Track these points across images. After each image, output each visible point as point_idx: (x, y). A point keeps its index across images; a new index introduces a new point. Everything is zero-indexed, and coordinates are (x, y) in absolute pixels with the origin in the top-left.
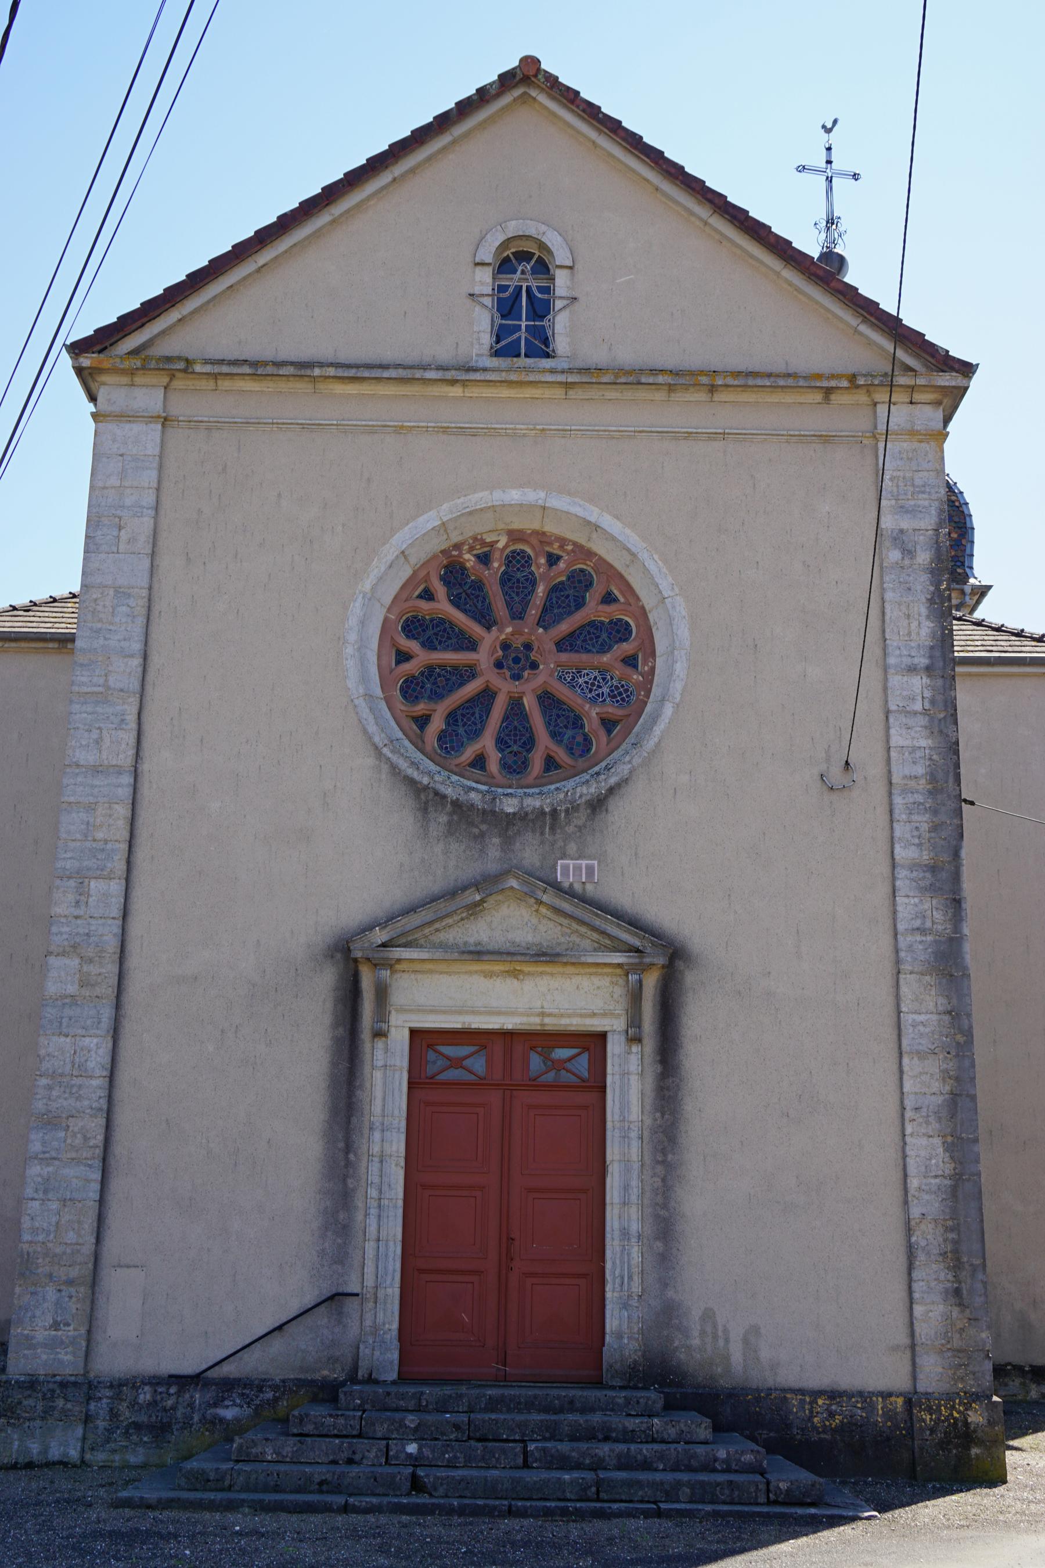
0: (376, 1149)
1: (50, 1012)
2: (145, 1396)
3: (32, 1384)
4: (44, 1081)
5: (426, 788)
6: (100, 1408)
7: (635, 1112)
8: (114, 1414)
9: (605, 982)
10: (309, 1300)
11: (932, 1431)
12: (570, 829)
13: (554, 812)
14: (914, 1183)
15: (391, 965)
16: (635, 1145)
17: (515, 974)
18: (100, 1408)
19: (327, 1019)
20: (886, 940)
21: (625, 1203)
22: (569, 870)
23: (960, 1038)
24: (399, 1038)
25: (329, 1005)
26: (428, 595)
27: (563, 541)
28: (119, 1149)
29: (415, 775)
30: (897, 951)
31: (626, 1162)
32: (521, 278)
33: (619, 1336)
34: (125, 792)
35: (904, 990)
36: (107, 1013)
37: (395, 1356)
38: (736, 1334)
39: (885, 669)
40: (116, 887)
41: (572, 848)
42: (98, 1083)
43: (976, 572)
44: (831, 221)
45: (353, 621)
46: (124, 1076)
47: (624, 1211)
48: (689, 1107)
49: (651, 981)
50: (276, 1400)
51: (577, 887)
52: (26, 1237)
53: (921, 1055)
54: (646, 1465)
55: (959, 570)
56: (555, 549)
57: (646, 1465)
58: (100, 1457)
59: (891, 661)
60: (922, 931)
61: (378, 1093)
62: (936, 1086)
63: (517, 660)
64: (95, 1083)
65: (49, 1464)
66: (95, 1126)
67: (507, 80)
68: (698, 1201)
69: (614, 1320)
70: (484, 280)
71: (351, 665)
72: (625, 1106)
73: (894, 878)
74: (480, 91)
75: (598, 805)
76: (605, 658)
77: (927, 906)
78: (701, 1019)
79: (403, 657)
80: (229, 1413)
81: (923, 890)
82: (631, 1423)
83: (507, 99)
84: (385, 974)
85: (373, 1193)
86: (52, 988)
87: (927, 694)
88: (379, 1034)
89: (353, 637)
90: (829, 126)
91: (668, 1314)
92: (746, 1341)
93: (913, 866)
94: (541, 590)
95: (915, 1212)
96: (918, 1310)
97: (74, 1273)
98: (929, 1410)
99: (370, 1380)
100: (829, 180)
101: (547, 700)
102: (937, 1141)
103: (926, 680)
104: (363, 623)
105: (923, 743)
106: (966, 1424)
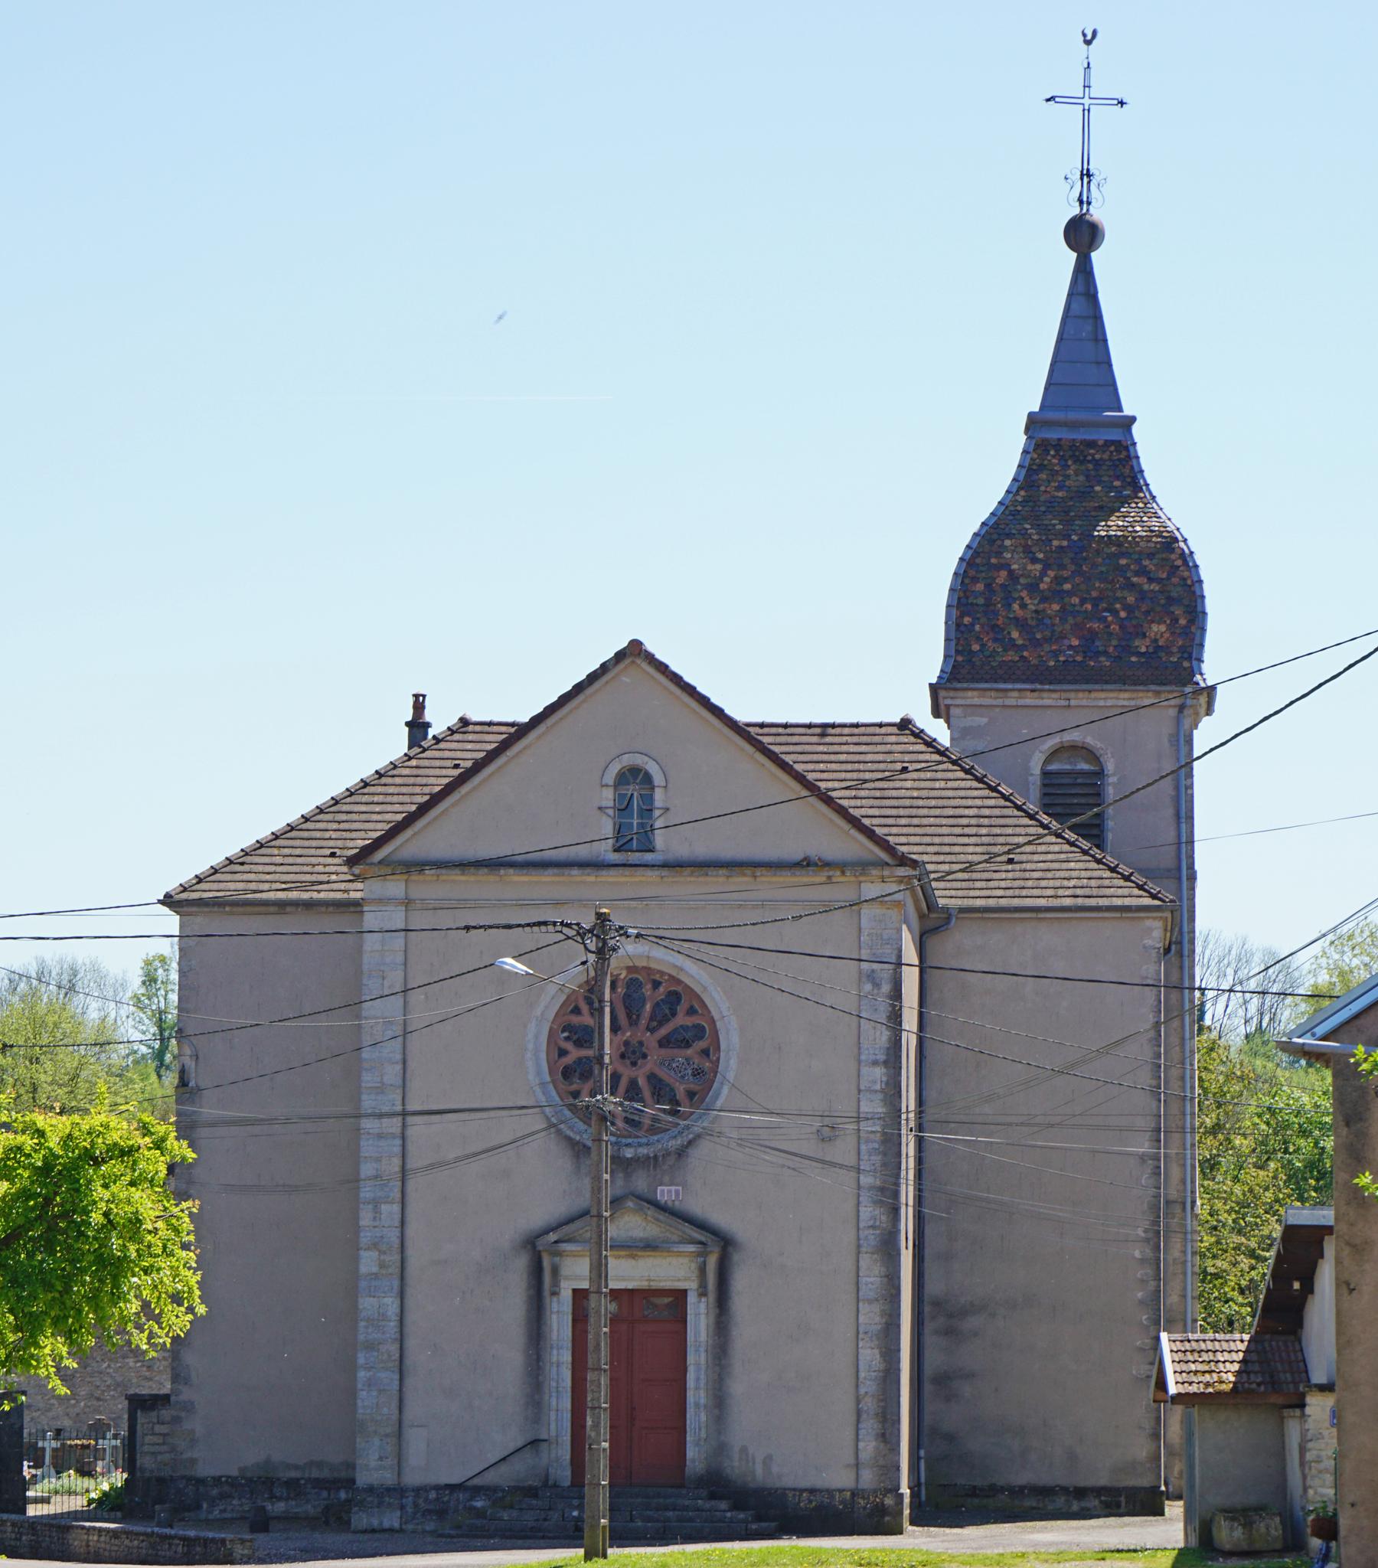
0: (554, 1359)
1: (363, 1284)
2: (433, 1495)
3: (371, 1489)
4: (363, 1324)
5: (578, 1142)
6: (409, 1501)
7: (703, 1337)
8: (416, 1505)
9: (686, 1260)
10: (520, 1444)
11: (865, 1508)
12: (666, 1167)
13: (656, 1157)
14: (862, 1375)
15: (560, 1254)
16: (703, 1355)
17: (633, 1257)
18: (409, 1501)
19: (524, 1285)
20: (853, 1232)
21: (697, 1388)
22: (665, 1193)
23: (893, 1291)
24: (566, 1294)
25: (525, 1276)
26: (577, 1011)
27: (662, 973)
28: (408, 1362)
29: (572, 1135)
30: (859, 1239)
31: (697, 1365)
32: (633, 790)
33: (693, 1461)
34: (397, 1150)
35: (862, 1263)
36: (396, 1283)
37: (568, 1473)
38: (759, 1460)
39: (859, 1062)
40: (396, 1208)
41: (666, 1179)
42: (393, 1325)
43: (1205, 667)
44: (1086, 174)
45: (530, 1036)
46: (410, 1318)
47: (697, 1393)
48: (735, 1333)
49: (712, 1261)
50: (504, 1497)
51: (670, 1203)
52: (360, 1411)
53: (870, 1302)
54: (691, 1520)
55: (1186, 664)
56: (657, 977)
57: (691, 1520)
58: (410, 1527)
59: (863, 1057)
60: (873, 1227)
61: (555, 1326)
62: (877, 1319)
63: (634, 1052)
64: (392, 1324)
65: (384, 1531)
66: (394, 1348)
67: (620, 656)
68: (738, 1387)
69: (691, 1453)
70: (608, 797)
71: (530, 1064)
72: (697, 1334)
73: (859, 1196)
74: (603, 665)
75: (681, 1153)
76: (689, 1052)
77: (877, 1212)
78: (742, 1281)
79: (563, 1053)
80: (479, 1504)
81: (875, 1202)
82: (687, 1503)
83: (621, 666)
84: (557, 1259)
85: (554, 1384)
86: (363, 1269)
87: (884, 1079)
88: (554, 1294)
89: (531, 1046)
90: (1089, 37)
91: (721, 1449)
92: (764, 1462)
93: (871, 1188)
94: (648, 1007)
95: (862, 1391)
96: (861, 1445)
97: (389, 1430)
98: (863, 1498)
99: (555, 1486)
100: (1087, 111)
101: (652, 1078)
102: (877, 1351)
103: (884, 1070)
104: (536, 1037)
105: (880, 1110)
106: (883, 1505)
